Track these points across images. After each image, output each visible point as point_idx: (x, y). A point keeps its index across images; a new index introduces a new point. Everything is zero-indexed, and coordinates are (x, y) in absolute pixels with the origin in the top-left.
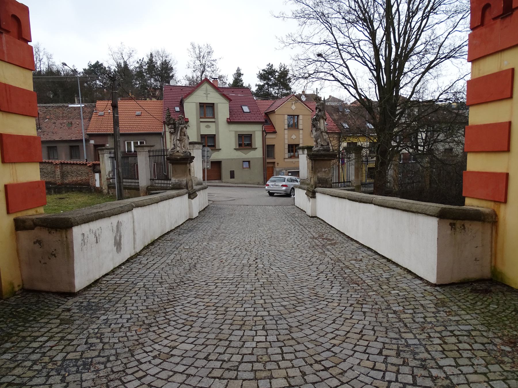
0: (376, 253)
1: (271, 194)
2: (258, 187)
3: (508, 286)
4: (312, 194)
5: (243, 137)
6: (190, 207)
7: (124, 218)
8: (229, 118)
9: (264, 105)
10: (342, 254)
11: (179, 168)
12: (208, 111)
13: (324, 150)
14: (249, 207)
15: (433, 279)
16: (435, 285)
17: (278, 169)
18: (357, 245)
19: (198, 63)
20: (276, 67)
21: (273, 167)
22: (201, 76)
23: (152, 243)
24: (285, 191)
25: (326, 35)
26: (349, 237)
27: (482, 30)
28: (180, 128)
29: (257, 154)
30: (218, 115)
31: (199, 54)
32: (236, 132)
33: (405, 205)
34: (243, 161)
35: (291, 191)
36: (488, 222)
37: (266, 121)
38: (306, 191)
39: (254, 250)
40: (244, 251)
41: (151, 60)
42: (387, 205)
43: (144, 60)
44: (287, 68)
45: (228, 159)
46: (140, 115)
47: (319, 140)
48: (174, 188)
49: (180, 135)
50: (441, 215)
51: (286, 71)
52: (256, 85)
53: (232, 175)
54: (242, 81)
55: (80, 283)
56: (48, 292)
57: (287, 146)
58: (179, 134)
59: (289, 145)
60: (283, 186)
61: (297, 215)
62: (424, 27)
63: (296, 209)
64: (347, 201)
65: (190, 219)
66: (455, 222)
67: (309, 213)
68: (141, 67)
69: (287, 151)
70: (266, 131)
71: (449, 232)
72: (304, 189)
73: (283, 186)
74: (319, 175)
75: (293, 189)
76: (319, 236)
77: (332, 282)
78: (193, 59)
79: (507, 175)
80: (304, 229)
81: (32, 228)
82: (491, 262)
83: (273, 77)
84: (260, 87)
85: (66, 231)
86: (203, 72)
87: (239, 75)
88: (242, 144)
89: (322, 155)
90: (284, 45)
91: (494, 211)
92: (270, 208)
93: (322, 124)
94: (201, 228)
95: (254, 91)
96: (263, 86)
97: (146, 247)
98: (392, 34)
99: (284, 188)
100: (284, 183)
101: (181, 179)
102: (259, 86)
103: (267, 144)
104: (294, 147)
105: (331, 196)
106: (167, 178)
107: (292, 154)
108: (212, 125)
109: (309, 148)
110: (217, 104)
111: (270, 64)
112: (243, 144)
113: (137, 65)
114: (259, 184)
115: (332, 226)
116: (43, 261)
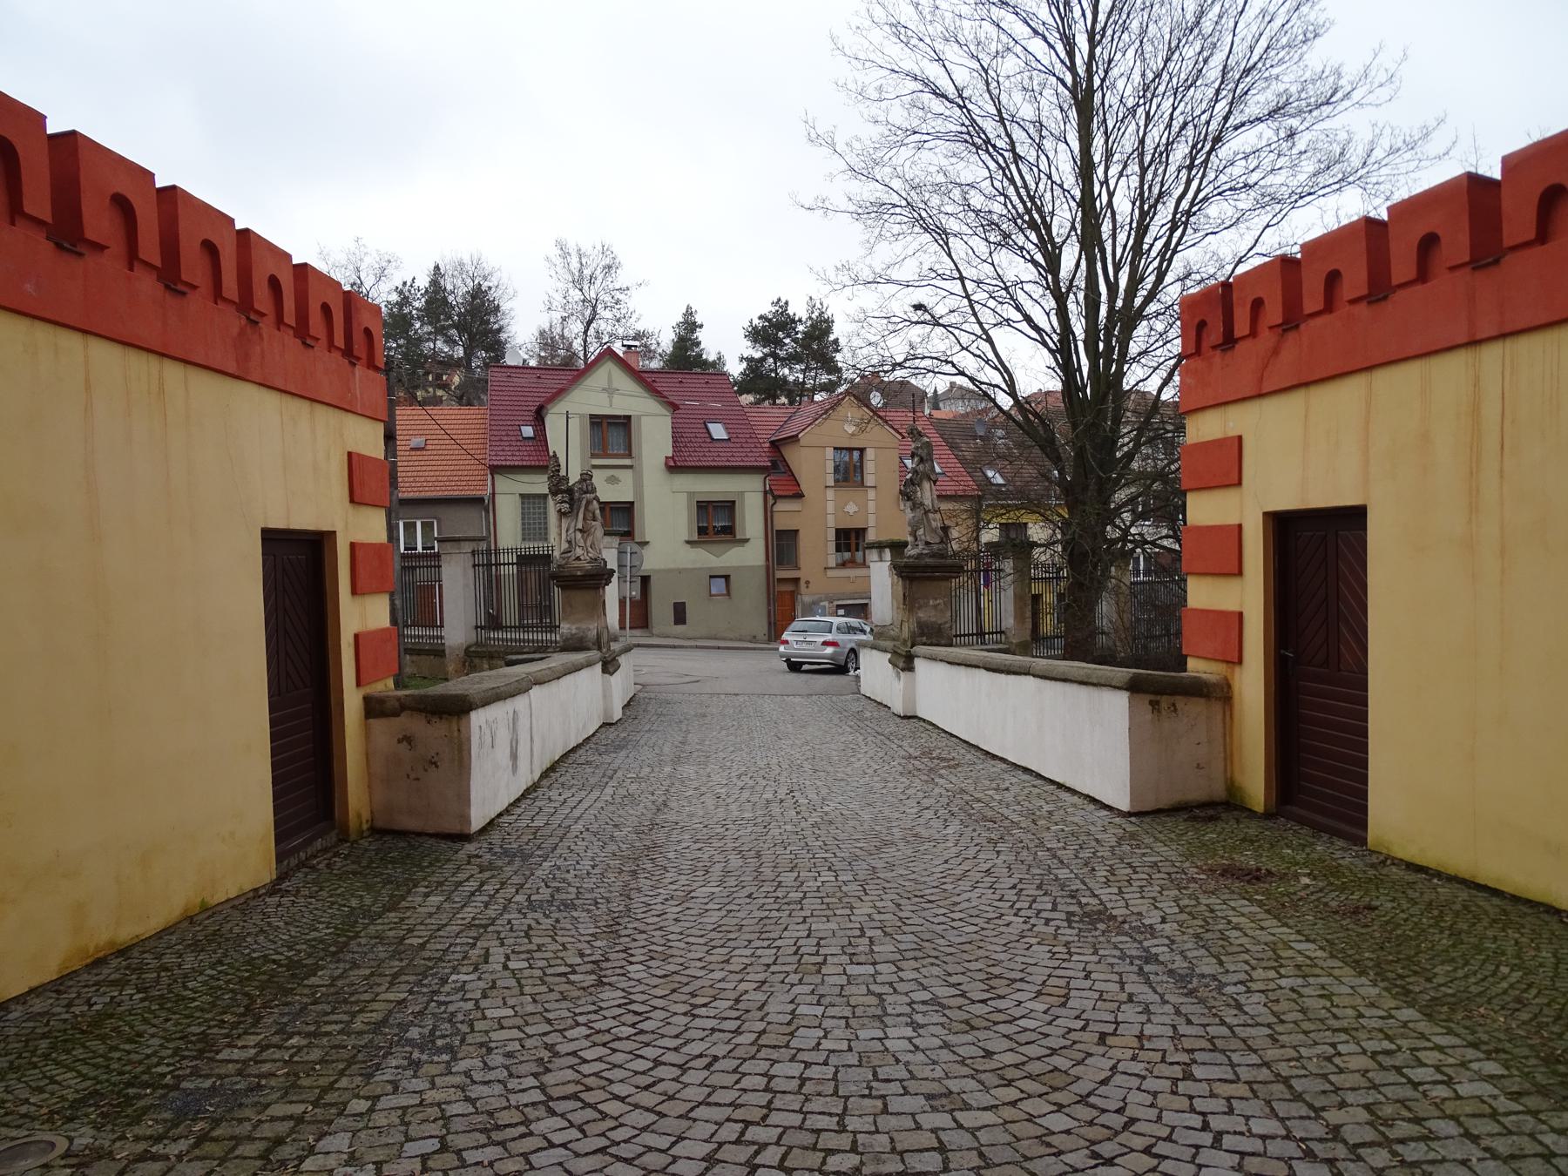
0: (1039, 776)
1: (795, 667)
2: (754, 649)
3: (1250, 810)
4: (905, 663)
5: (711, 509)
6: (606, 695)
7: (520, 703)
8: (673, 458)
9: (771, 417)
10: (970, 781)
11: (580, 597)
12: (615, 437)
13: (933, 555)
14: (741, 699)
15: (1124, 804)
16: (1130, 814)
17: (807, 599)
18: (1004, 766)
19: (576, 295)
20: (798, 310)
21: (793, 592)
22: (586, 332)
23: (552, 768)
24: (832, 657)
25: (933, 255)
26: (987, 753)
27: (1196, 363)
28: (584, 502)
29: (749, 555)
30: (640, 447)
31: (581, 271)
32: (691, 494)
33: (1082, 672)
34: (711, 577)
35: (848, 657)
36: (1216, 698)
37: (774, 465)
38: (889, 656)
39: (783, 779)
40: (760, 780)
41: (435, 283)
42: (1054, 675)
43: (416, 285)
44: (829, 313)
45: (669, 571)
46: (422, 449)
47: (920, 532)
48: (566, 649)
49: (584, 519)
50: (1133, 687)
51: (827, 321)
52: (742, 359)
53: (680, 614)
54: (698, 344)
55: (477, 821)
56: (419, 834)
57: (832, 535)
58: (581, 516)
59: (838, 531)
60: (826, 643)
61: (868, 714)
62: (1178, 243)
63: (864, 702)
64: (983, 671)
65: (605, 725)
66: (1158, 698)
67: (898, 708)
68: (405, 301)
69: (832, 546)
70: (776, 493)
71: (1149, 716)
72: (886, 651)
73: (826, 643)
74: (921, 614)
75: (854, 652)
76: (923, 753)
77: (946, 820)
78: (561, 286)
79: (1241, 615)
80: (887, 742)
81: (396, 714)
82: (1225, 771)
83: (788, 336)
84: (754, 365)
85: (459, 718)
86: (589, 323)
87: (690, 325)
88: (707, 528)
89: (927, 566)
90: (829, 288)
91: (1226, 679)
92: (798, 699)
93: (927, 494)
94: (642, 742)
95: (736, 375)
96: (763, 359)
97: (545, 774)
98: (1099, 265)
99: (829, 650)
100: (829, 637)
101: (584, 626)
102: (750, 360)
103: (776, 528)
104: (853, 535)
105: (949, 663)
106: (553, 628)
107: (847, 555)
108: (626, 476)
109: (897, 547)
110: (639, 417)
111: (779, 300)
112: (711, 529)
113: (394, 297)
114: (754, 639)
115: (952, 735)
116: (413, 776)
